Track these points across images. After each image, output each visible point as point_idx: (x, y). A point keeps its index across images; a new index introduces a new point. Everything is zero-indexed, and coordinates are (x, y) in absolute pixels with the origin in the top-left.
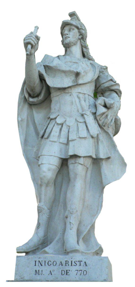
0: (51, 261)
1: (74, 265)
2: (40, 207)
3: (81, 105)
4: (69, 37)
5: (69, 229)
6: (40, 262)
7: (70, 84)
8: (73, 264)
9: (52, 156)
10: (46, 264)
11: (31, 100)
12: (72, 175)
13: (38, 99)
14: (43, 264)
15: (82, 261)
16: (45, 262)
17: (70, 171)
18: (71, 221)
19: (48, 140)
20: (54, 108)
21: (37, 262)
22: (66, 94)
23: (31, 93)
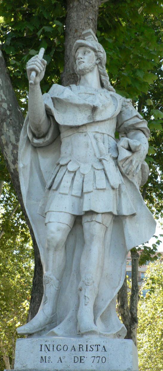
1: (90, 350)
3: (98, 148)
4: (84, 62)
7: (85, 122)
8: (89, 348)
9: (61, 212)
10: (55, 349)
11: (36, 141)
12: (87, 236)
13: (45, 140)
14: (51, 349)
15: (100, 345)
16: (53, 346)
17: (84, 231)
18: (86, 295)
19: (57, 192)
21: (43, 347)
22: (80, 134)
23: (35, 132)
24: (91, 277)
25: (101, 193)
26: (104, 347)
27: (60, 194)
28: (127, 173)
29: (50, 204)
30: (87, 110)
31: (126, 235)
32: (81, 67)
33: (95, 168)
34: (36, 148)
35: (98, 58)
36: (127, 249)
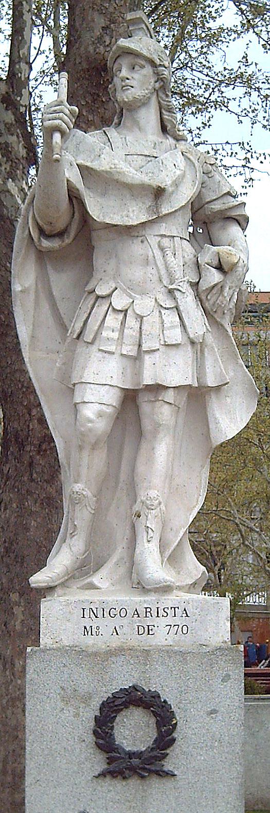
0: (115, 609)
1: (163, 616)
2: (77, 492)
3: (167, 268)
4: (132, 87)
5: (145, 541)
6: (93, 611)
7: (144, 218)
8: (161, 612)
9: (105, 385)
11: (46, 243)
12: (147, 425)
13: (63, 241)
14: (100, 614)
15: (178, 608)
16: (103, 610)
17: (142, 417)
18: (148, 525)
19: (94, 348)
20: (103, 270)
21: (87, 612)
22: (133, 240)
23: (45, 227)
24: (156, 496)
25: (173, 352)
26: (185, 610)
27: (100, 352)
28: (214, 310)
29: (83, 368)
30: (147, 194)
31: (211, 419)
32: (126, 96)
33: (161, 306)
34: (42, 256)
35: (158, 79)
36: (212, 445)
